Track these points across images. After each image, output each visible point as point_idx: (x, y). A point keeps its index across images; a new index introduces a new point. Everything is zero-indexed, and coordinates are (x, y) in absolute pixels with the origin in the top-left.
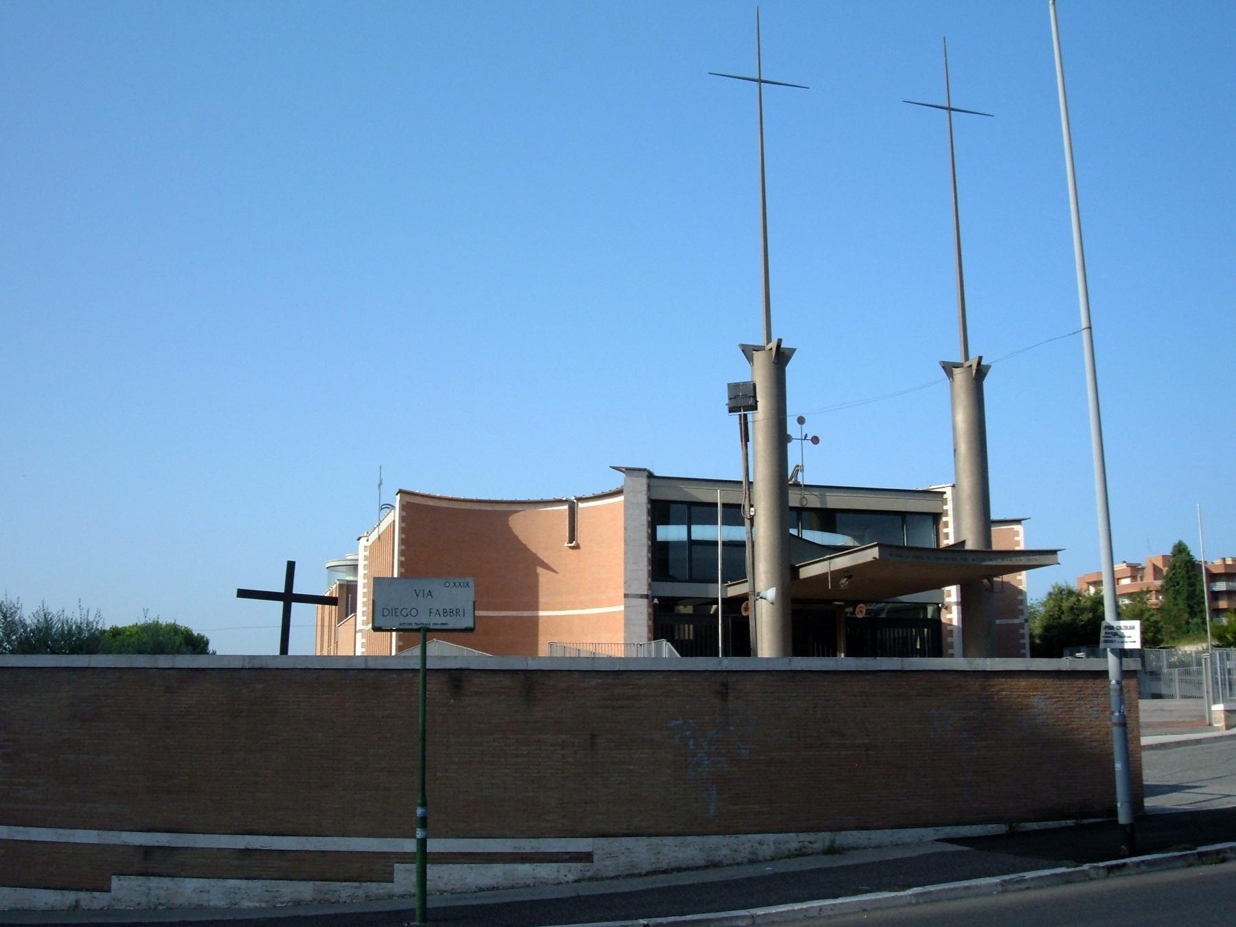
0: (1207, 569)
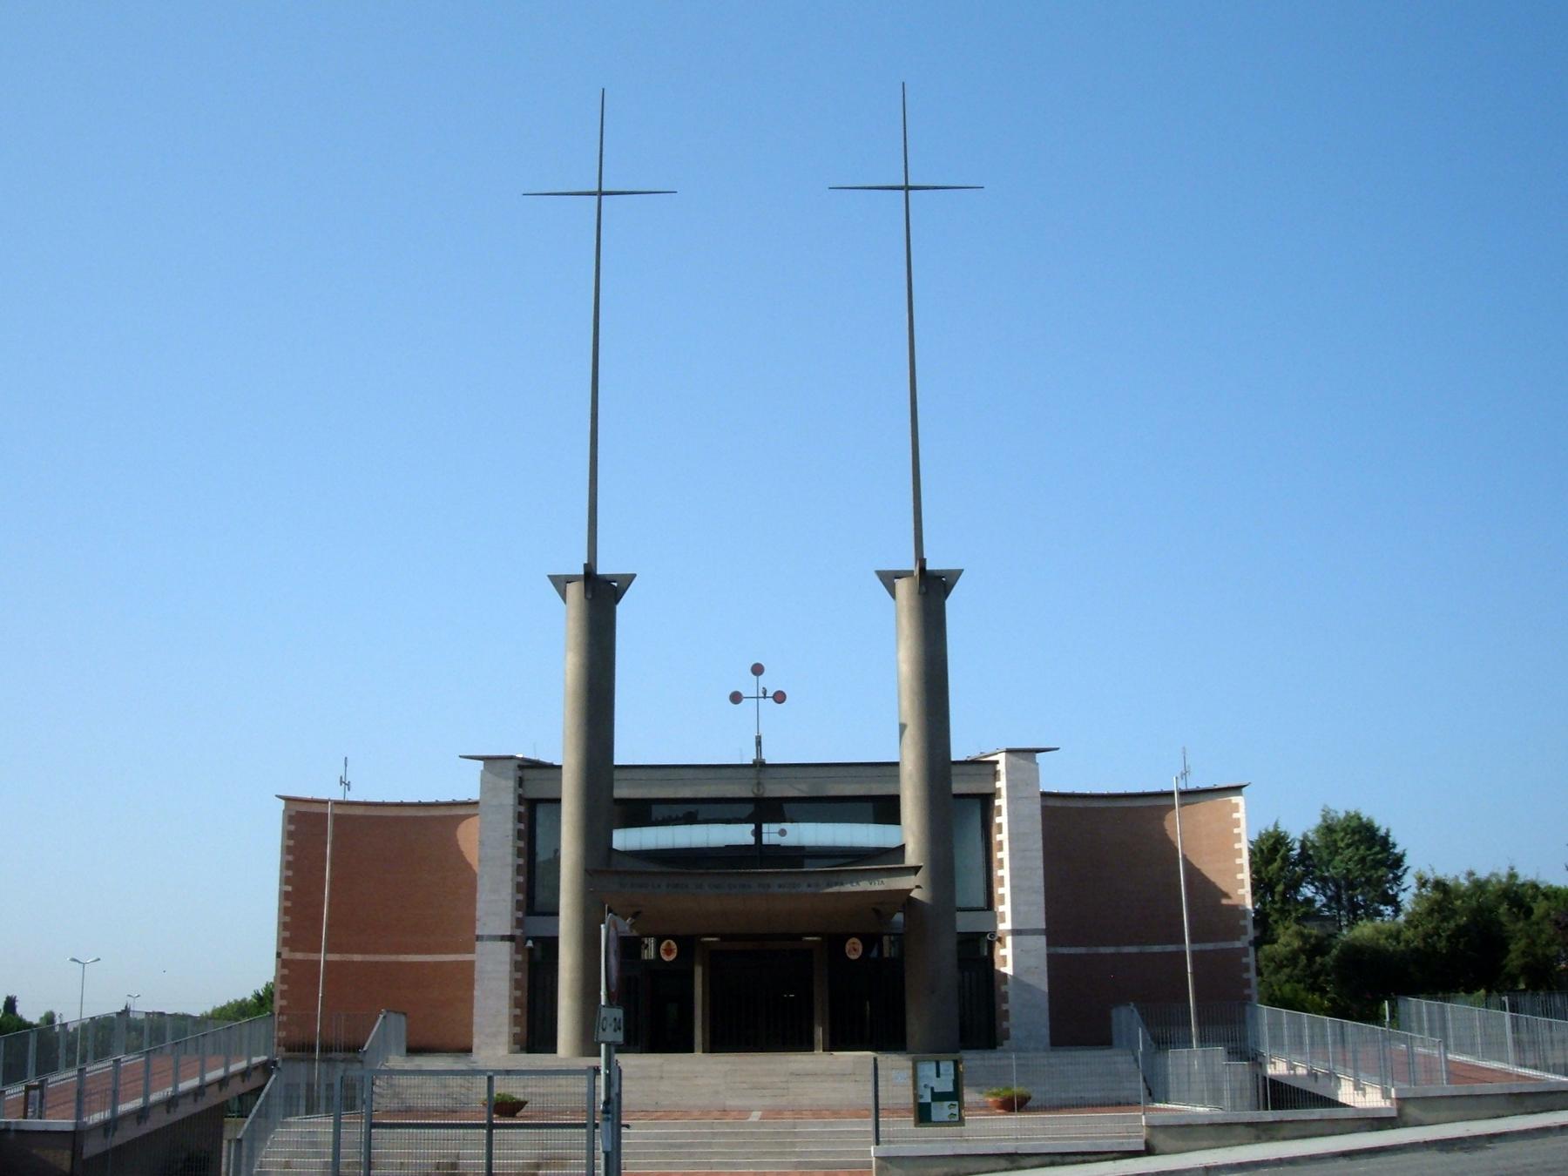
0: (1194, 874)
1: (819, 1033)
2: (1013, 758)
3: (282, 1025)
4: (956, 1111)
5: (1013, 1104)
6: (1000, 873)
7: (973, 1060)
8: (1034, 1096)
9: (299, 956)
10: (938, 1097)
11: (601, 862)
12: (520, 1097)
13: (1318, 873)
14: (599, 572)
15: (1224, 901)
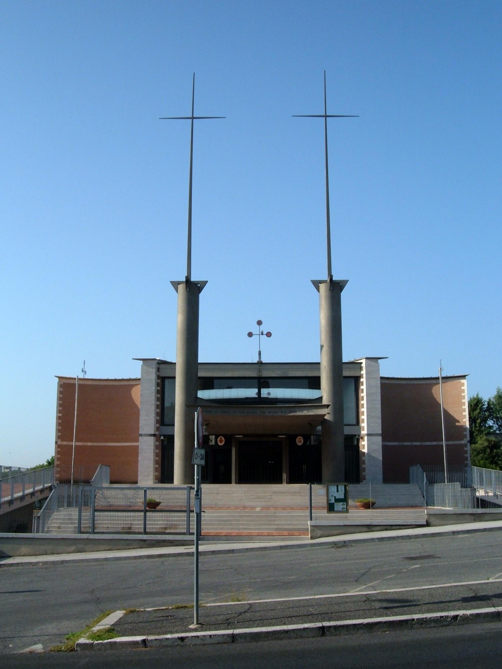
0: (445, 411)
1: (285, 476)
2: (368, 361)
3: (58, 472)
4: (345, 507)
5: (367, 506)
6: (362, 410)
7: (351, 487)
8: (377, 503)
9: (65, 443)
10: (337, 500)
11: (192, 402)
12: (158, 501)
13: (495, 415)
14: (192, 280)
15: (457, 424)
